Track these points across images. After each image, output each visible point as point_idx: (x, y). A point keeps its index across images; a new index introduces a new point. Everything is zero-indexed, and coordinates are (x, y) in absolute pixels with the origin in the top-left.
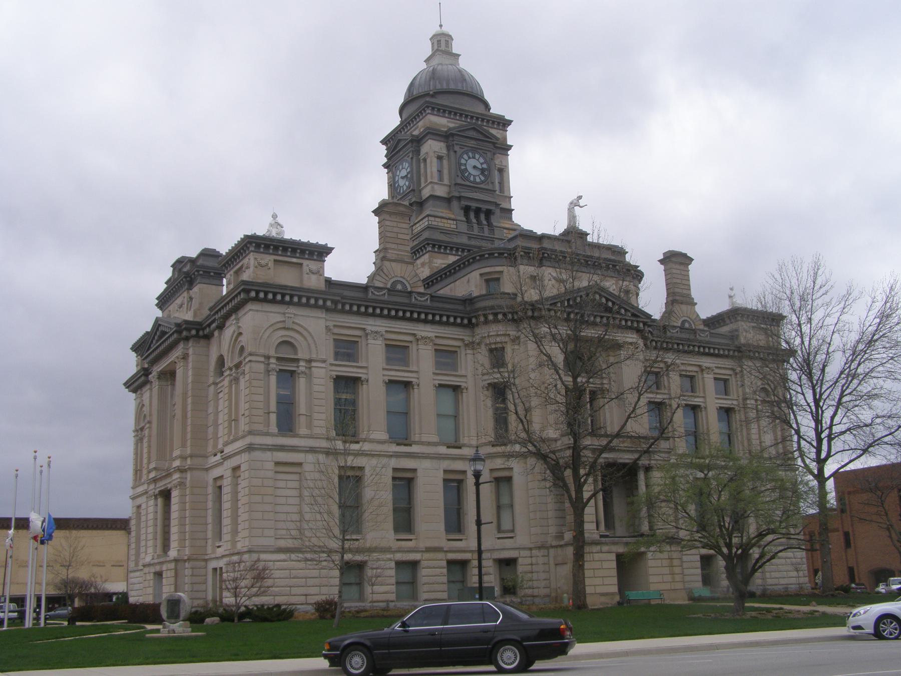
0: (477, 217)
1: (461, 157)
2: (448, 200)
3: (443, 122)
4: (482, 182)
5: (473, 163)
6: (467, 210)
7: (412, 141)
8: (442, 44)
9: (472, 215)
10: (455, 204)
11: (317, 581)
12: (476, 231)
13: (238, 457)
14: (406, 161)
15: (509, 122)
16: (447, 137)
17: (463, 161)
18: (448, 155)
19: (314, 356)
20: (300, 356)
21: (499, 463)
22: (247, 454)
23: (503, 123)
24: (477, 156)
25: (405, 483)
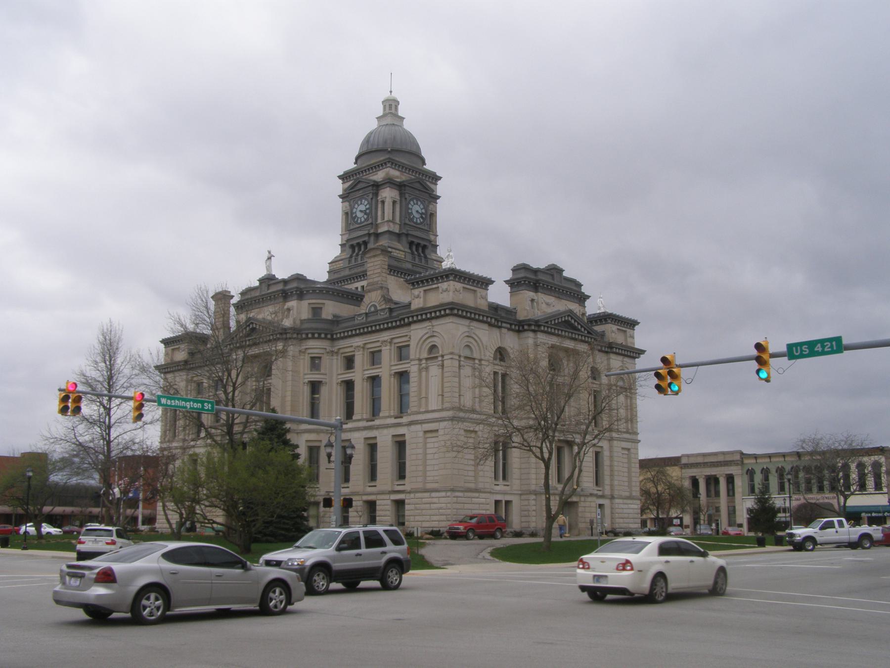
0: (417, 250)
1: (409, 203)
2: (399, 236)
3: (395, 173)
4: (421, 223)
5: (416, 208)
6: (411, 244)
7: (373, 185)
8: (391, 106)
9: (414, 248)
10: (404, 239)
11: (423, 506)
12: (417, 261)
13: (437, 424)
14: (366, 199)
15: (440, 178)
16: (401, 187)
17: (410, 206)
18: (401, 201)
19: (483, 357)
20: (475, 356)
21: (312, 437)
22: (450, 423)
23: (435, 178)
25: (372, 448)
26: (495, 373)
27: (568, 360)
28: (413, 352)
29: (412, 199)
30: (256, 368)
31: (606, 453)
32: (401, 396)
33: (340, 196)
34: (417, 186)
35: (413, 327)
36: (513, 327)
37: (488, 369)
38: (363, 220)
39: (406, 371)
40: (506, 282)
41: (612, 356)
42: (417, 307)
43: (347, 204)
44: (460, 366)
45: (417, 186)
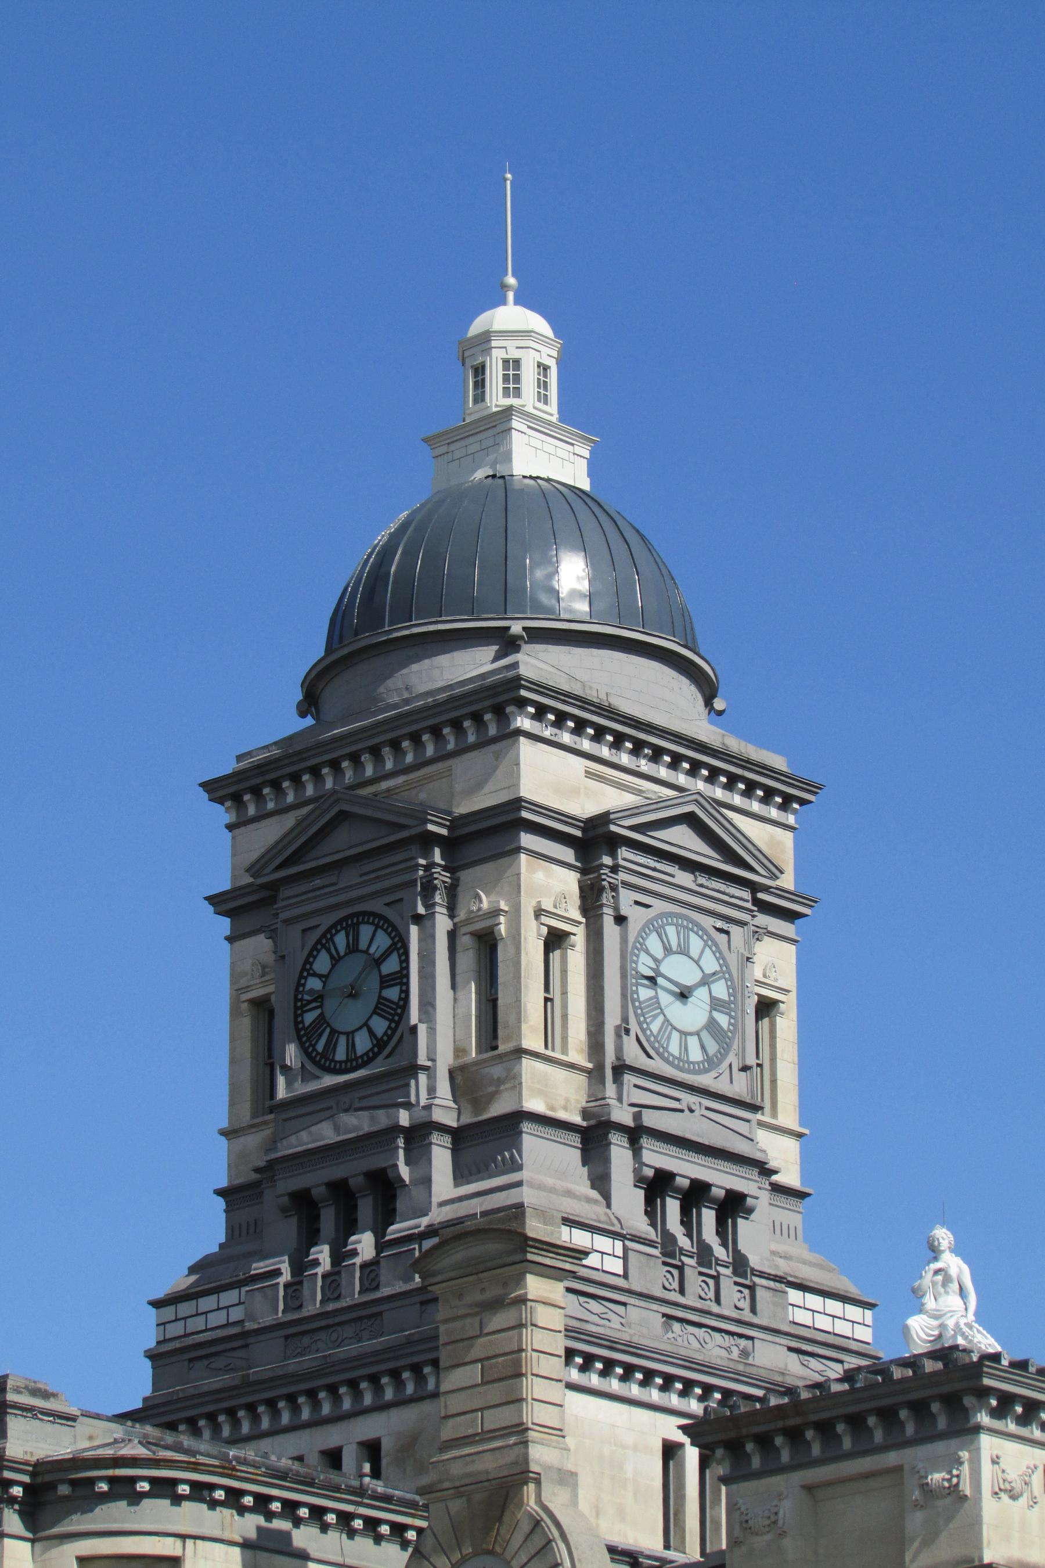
24: (696, 944)
29: (653, 926)
33: (218, 902)
34: (682, 839)
38: (363, 1043)
40: (219, 1192)
43: (260, 946)
45: (682, 839)
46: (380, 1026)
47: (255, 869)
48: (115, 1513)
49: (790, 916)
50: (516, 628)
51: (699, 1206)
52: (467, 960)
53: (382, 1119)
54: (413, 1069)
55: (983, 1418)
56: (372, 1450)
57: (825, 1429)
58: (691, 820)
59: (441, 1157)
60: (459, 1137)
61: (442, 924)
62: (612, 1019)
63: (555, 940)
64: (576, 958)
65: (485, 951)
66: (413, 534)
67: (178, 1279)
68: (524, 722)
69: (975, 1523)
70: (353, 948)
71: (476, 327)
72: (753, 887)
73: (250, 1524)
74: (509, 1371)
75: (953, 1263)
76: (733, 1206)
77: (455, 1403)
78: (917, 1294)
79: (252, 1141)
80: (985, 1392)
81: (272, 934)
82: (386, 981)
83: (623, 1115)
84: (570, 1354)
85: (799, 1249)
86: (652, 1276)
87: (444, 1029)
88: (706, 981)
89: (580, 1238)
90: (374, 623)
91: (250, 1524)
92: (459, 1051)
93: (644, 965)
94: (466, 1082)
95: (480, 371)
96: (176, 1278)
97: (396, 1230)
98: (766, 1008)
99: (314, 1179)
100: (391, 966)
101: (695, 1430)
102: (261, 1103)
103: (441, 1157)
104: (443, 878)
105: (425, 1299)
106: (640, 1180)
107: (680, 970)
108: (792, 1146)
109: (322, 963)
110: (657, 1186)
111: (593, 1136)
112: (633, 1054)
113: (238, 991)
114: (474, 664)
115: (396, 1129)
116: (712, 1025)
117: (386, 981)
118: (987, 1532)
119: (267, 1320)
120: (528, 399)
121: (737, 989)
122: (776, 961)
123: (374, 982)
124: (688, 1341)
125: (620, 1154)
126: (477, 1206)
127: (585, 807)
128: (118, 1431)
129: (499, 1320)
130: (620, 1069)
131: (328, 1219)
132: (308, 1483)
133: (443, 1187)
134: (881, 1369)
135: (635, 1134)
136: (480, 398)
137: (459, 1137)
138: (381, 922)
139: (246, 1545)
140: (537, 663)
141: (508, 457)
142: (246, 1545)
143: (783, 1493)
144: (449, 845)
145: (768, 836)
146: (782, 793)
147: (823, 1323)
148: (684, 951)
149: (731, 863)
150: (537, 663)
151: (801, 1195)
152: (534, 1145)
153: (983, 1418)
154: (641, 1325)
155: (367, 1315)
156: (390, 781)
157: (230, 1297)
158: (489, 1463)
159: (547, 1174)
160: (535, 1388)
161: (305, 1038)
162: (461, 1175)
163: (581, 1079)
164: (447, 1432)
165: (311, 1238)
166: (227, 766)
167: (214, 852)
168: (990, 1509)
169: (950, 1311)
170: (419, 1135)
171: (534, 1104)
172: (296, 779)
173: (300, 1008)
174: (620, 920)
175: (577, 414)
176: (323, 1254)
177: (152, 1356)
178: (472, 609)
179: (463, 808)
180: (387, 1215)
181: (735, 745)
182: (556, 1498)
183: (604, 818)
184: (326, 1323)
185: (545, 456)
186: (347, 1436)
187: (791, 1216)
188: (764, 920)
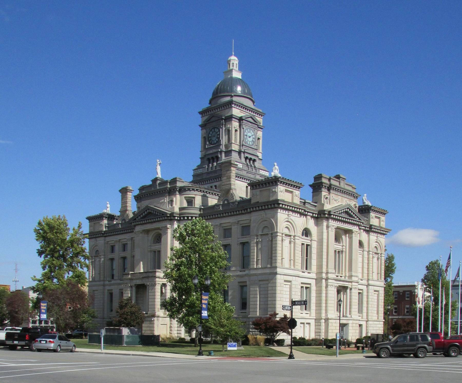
24: (251, 131)
26: (303, 244)
27: (346, 237)
28: (253, 230)
29: (247, 129)
30: (151, 236)
31: (365, 294)
32: (244, 257)
33: (200, 126)
34: (250, 120)
35: (253, 214)
36: (314, 215)
37: (299, 242)
38: (215, 142)
39: (247, 242)
40: (310, 186)
41: (330, 220)
42: (254, 202)
43: (204, 131)
44: (282, 240)
45: (250, 120)
46: (217, 140)
47: (204, 122)
48: (188, 192)
49: (262, 128)
50: (233, 95)
51: (251, 160)
52: (227, 132)
53: (217, 150)
54: (221, 145)
55: (279, 184)
56: (216, 186)
57: (262, 184)
58: (251, 117)
59: (223, 154)
60: (225, 152)
61: (224, 128)
62: (242, 140)
63: (236, 131)
64: (238, 133)
65: (228, 132)
66: (222, 84)
67: (195, 167)
68: (233, 106)
69: (277, 195)
70: (214, 131)
71: (229, 59)
72: (258, 125)
73: (202, 194)
74: (229, 178)
75: (277, 167)
76: (254, 161)
77: (224, 181)
78: (273, 170)
79: (203, 152)
80: (279, 181)
81: (206, 129)
82: (218, 135)
83: (243, 150)
84: (236, 176)
85: (261, 165)
86: (246, 168)
87: (224, 140)
88: (252, 136)
89: (238, 164)
90: (217, 94)
91: (202, 194)
92: (225, 143)
93: (246, 134)
94: (226, 146)
95: (229, 64)
96: (195, 167)
97: (218, 162)
98: (259, 139)
99: (210, 157)
100: (218, 133)
101: (249, 184)
102: (204, 149)
103: (223, 154)
104: (224, 123)
105: (221, 170)
106: (244, 157)
107: (249, 134)
108: (261, 154)
109: (211, 133)
110: (246, 158)
111: (240, 153)
112: (244, 144)
113: (202, 136)
114: (228, 99)
115: (219, 151)
116: (253, 141)
117: (218, 135)
118: (279, 196)
119: (205, 172)
120: (235, 68)
121: (256, 136)
122: (260, 134)
123: (216, 135)
124: (249, 175)
125: (242, 154)
126: (226, 160)
127: (240, 116)
128: (188, 183)
129: (229, 172)
130: (243, 145)
131: (211, 161)
132: (208, 189)
133: (223, 158)
134: (268, 178)
135: (244, 152)
136: (229, 67)
137: (225, 152)
138: (217, 128)
139: (202, 196)
140: (235, 99)
141: (232, 75)
142: (202, 196)
143: (257, 191)
144: (225, 119)
145: (260, 119)
146: (261, 114)
147: (263, 174)
148: (250, 132)
149: (255, 122)
150: (235, 99)
151: (261, 160)
152: (233, 153)
153: (279, 184)
154: (244, 173)
155: (215, 172)
156: (218, 112)
157: (201, 169)
158: (227, 187)
159: (234, 157)
160: (232, 180)
161: (209, 141)
162: (225, 157)
163: (238, 146)
164: (223, 184)
165: (209, 163)
166: (201, 110)
167: (199, 120)
168: (279, 193)
169: (276, 172)
170: (221, 152)
171: (233, 149)
172: (208, 112)
173: (209, 137)
174: (243, 128)
175: (240, 69)
176: (211, 165)
177: (193, 176)
178: (228, 93)
179: (226, 115)
180: (217, 161)
181: (256, 109)
182: (234, 192)
183: (241, 117)
184: (211, 172)
185: (237, 74)
186: (213, 185)
187: (261, 162)
188: (259, 129)
